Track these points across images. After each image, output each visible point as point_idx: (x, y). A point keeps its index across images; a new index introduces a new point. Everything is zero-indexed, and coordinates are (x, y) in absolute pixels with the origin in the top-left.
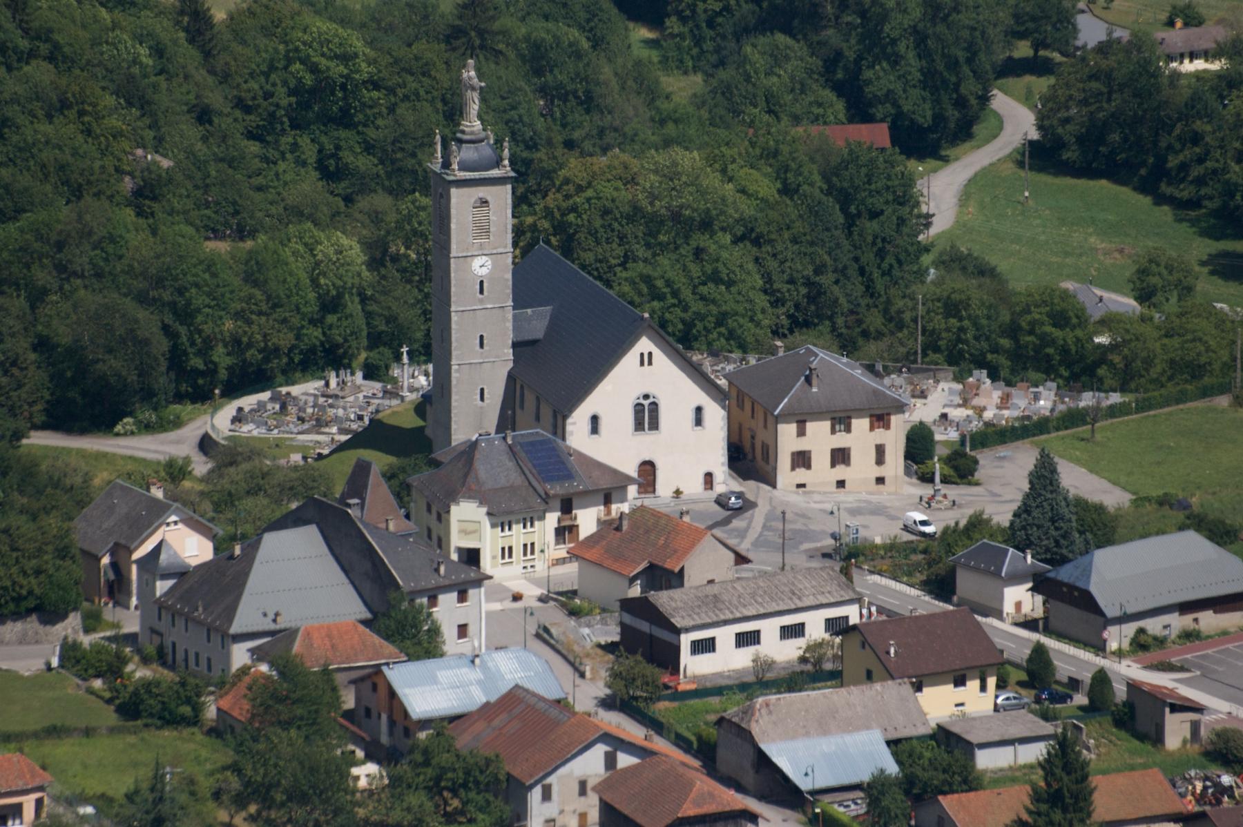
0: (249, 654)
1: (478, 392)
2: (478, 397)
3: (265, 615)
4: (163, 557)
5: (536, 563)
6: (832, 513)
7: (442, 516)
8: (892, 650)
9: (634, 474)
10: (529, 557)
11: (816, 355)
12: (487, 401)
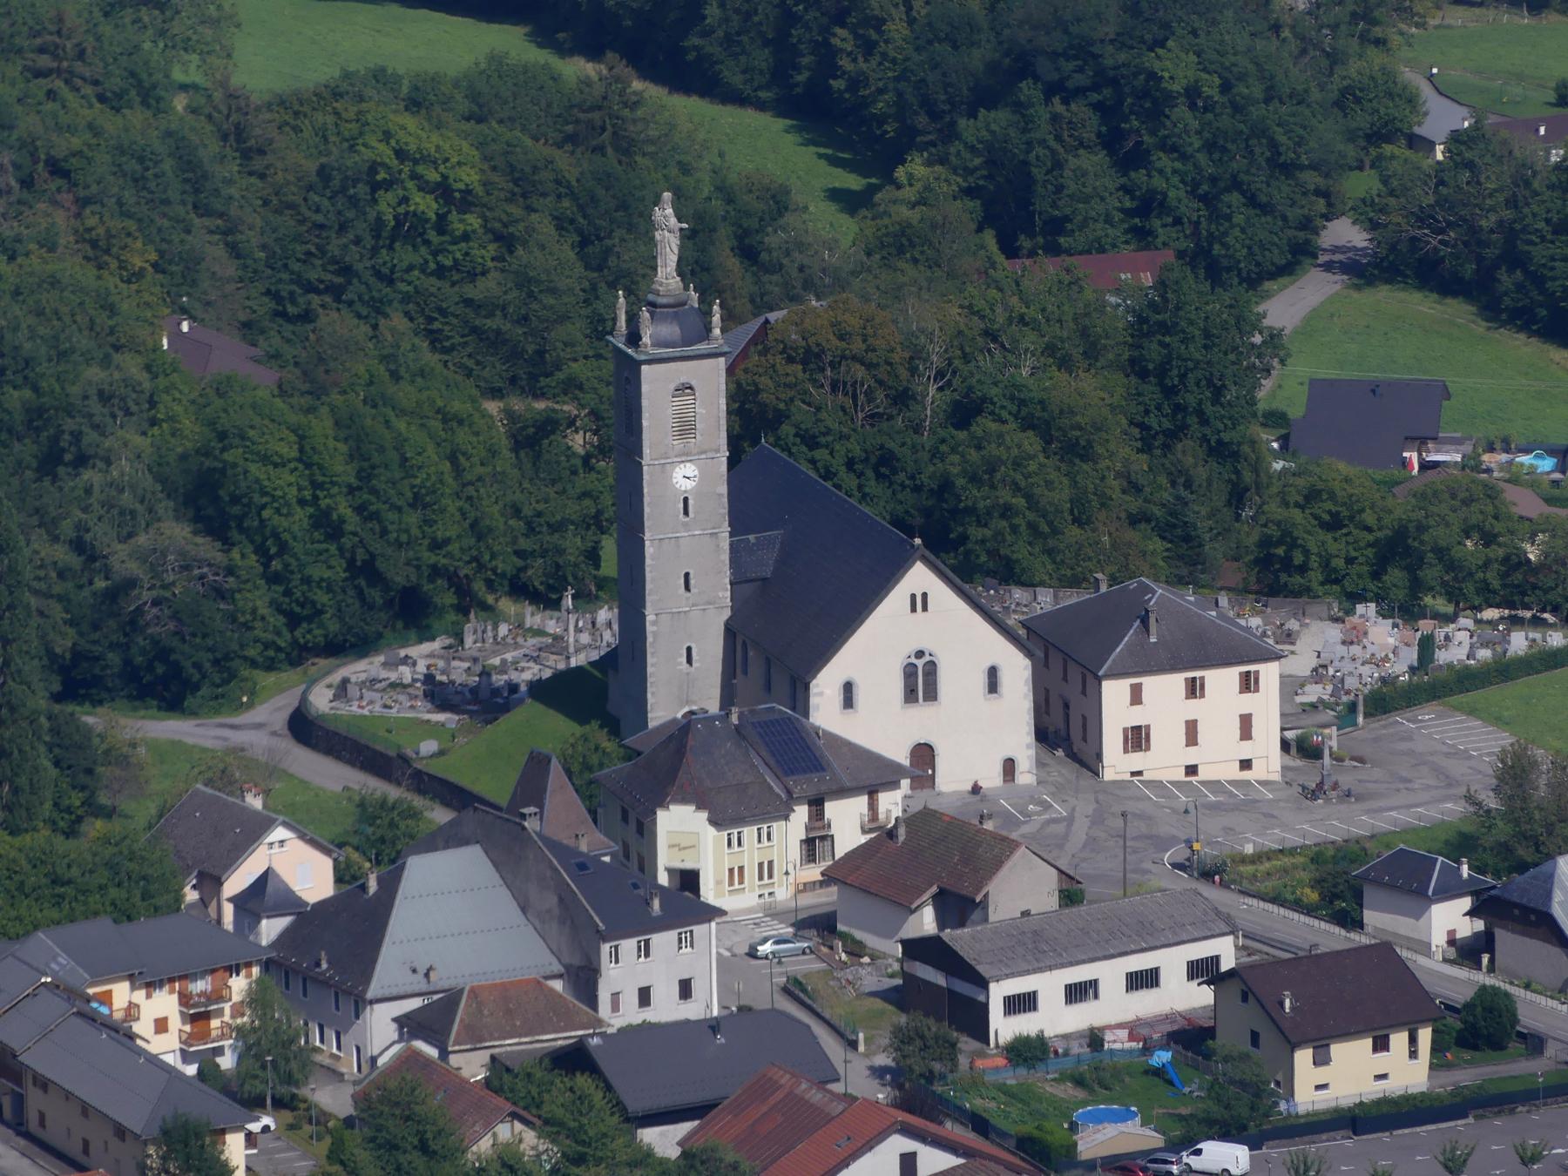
0: (394, 1026)
1: (684, 652)
2: (684, 659)
3: (414, 971)
4: (270, 889)
5: (776, 889)
6: (1186, 812)
7: (645, 830)
8: (1287, 1003)
9: (906, 762)
10: (766, 881)
11: (1154, 592)
12: (695, 664)
